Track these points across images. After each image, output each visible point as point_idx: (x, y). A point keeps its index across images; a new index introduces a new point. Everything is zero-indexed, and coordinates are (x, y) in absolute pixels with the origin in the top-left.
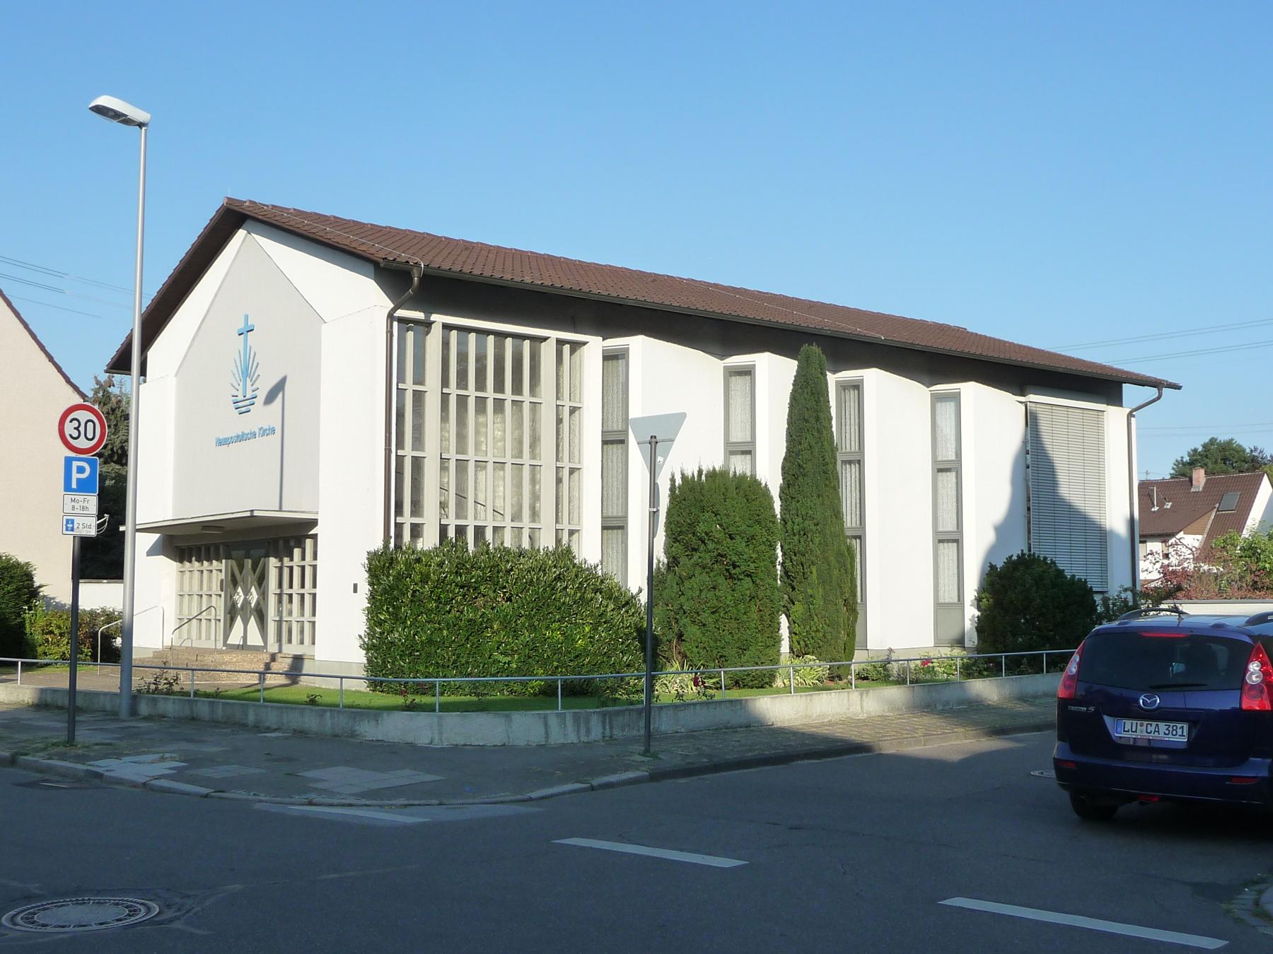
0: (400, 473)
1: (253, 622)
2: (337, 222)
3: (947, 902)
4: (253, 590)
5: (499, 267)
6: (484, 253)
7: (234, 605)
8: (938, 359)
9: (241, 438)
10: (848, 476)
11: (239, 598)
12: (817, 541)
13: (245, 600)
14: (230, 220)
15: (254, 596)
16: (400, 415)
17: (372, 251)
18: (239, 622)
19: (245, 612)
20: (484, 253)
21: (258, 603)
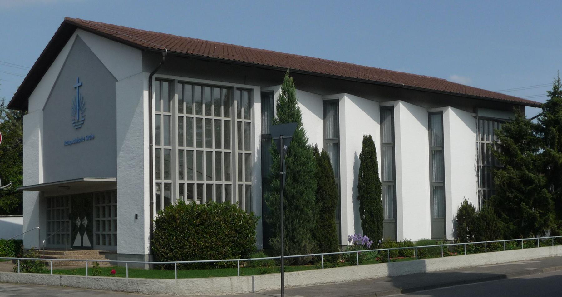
0: (158, 158)
1: (86, 236)
2: (104, 25)
3: (380, 179)
4: (85, 218)
5: (226, 54)
6: (204, 45)
7: (76, 226)
8: (433, 98)
9: (81, 141)
10: (385, 199)
11: (78, 223)
12: (360, 274)
13: (81, 224)
14: (68, 29)
15: (86, 222)
16: (158, 128)
17: (141, 43)
18: (79, 236)
19: (82, 230)
20: (204, 45)
21: (88, 226)
